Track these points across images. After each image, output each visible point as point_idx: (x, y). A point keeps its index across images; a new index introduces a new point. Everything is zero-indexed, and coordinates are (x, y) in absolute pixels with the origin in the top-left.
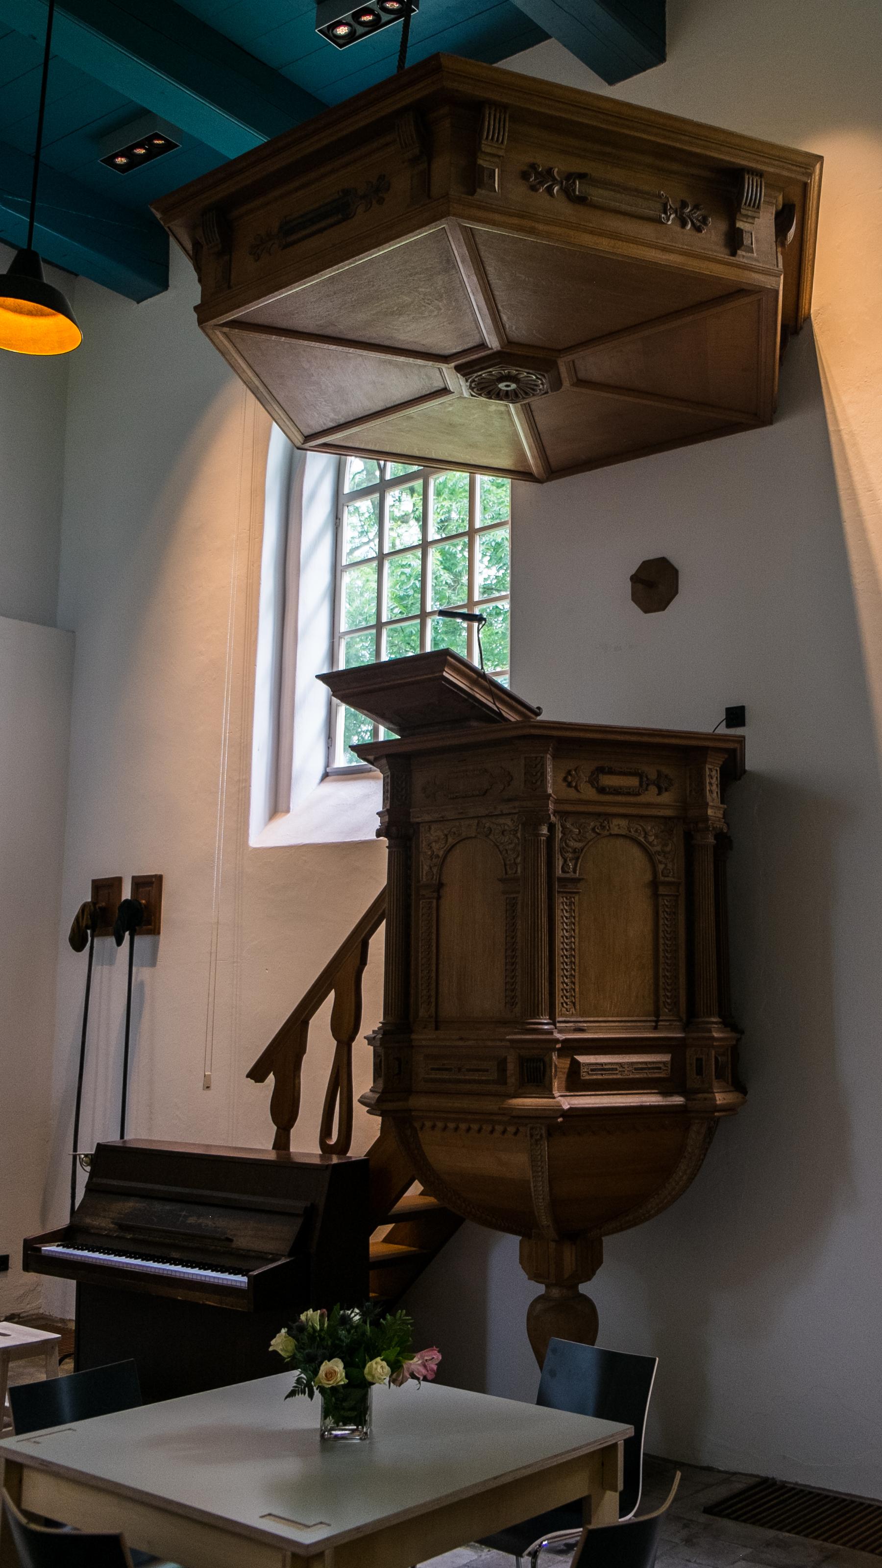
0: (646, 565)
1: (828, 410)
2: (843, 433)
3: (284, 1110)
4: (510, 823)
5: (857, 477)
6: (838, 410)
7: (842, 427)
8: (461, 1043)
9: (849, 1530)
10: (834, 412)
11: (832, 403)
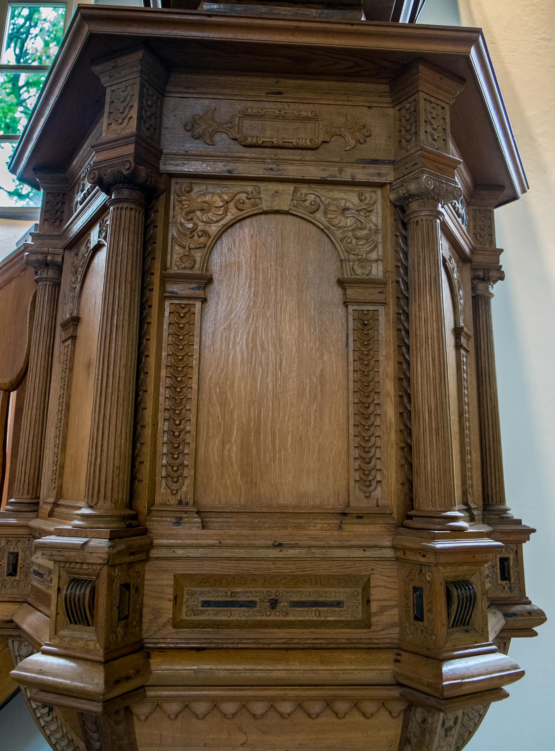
4: (356, 200)
8: (274, 553)
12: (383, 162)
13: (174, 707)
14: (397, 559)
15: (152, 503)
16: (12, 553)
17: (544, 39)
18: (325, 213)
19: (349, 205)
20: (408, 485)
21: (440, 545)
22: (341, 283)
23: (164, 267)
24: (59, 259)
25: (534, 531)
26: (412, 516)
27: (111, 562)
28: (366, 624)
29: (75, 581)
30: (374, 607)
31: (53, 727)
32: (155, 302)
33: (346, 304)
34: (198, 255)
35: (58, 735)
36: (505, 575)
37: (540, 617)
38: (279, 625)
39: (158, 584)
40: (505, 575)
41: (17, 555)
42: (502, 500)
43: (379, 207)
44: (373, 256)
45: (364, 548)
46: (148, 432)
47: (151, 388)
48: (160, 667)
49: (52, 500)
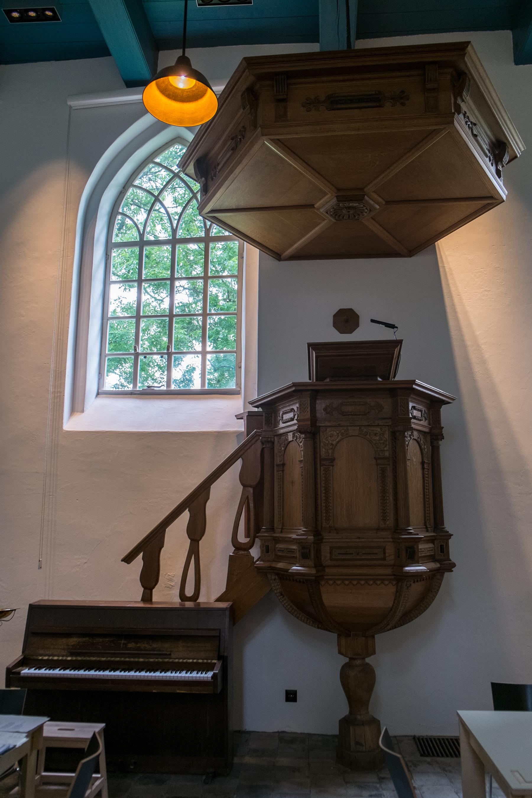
0: (351, 311)
1: (438, 256)
2: (446, 268)
3: (150, 578)
4: (379, 430)
5: (453, 289)
6: (444, 257)
7: (445, 265)
8: (358, 540)
9: (427, 745)
10: (441, 258)
11: (440, 254)
12: (388, 419)
13: (331, 582)
14: (393, 541)
15: (321, 527)
16: (266, 546)
17: (486, 291)
18: (370, 435)
19: (377, 432)
20: (396, 520)
21: (403, 537)
22: (375, 458)
23: (320, 457)
24: (273, 440)
25: (452, 535)
26: (398, 529)
27: (314, 543)
28: (384, 559)
29: (304, 548)
30: (387, 555)
31: (285, 602)
32: (319, 468)
33: (377, 465)
34: (330, 451)
35: (287, 604)
36: (442, 551)
37: (454, 565)
38: (360, 560)
39: (325, 549)
40: (442, 551)
41: (268, 546)
42: (443, 524)
43: (387, 432)
44: (386, 449)
45: (384, 538)
46: (319, 506)
47: (319, 494)
48: (328, 570)
49: (281, 527)
